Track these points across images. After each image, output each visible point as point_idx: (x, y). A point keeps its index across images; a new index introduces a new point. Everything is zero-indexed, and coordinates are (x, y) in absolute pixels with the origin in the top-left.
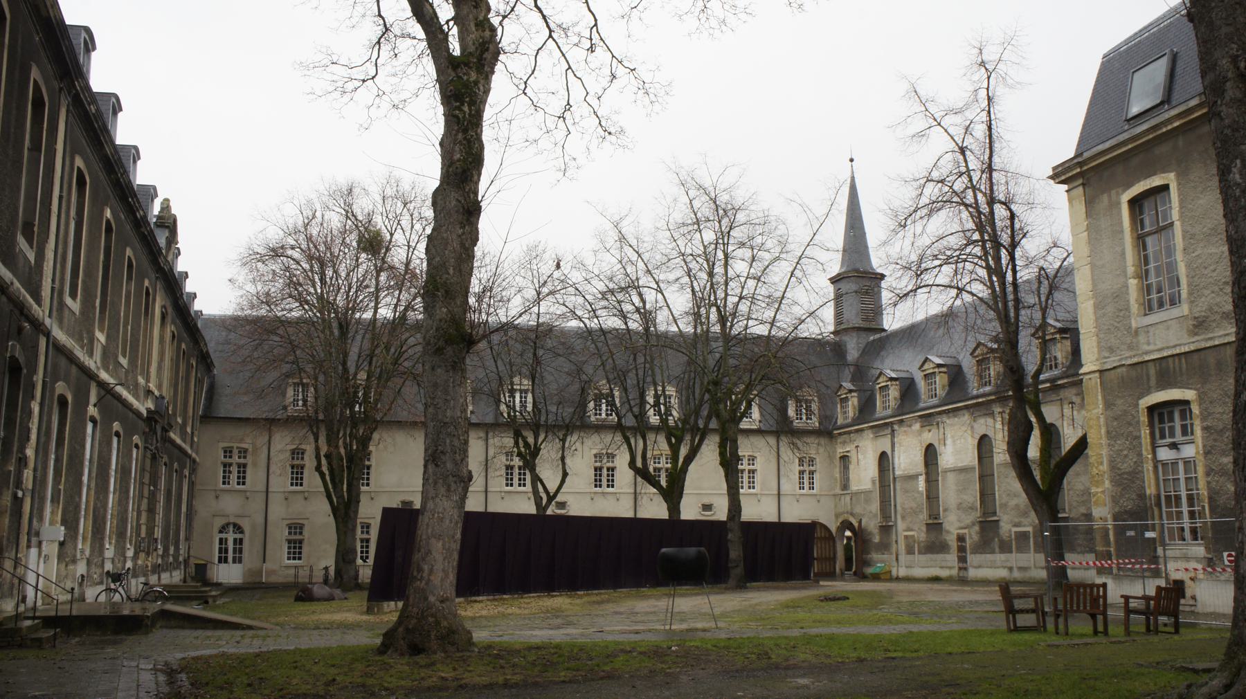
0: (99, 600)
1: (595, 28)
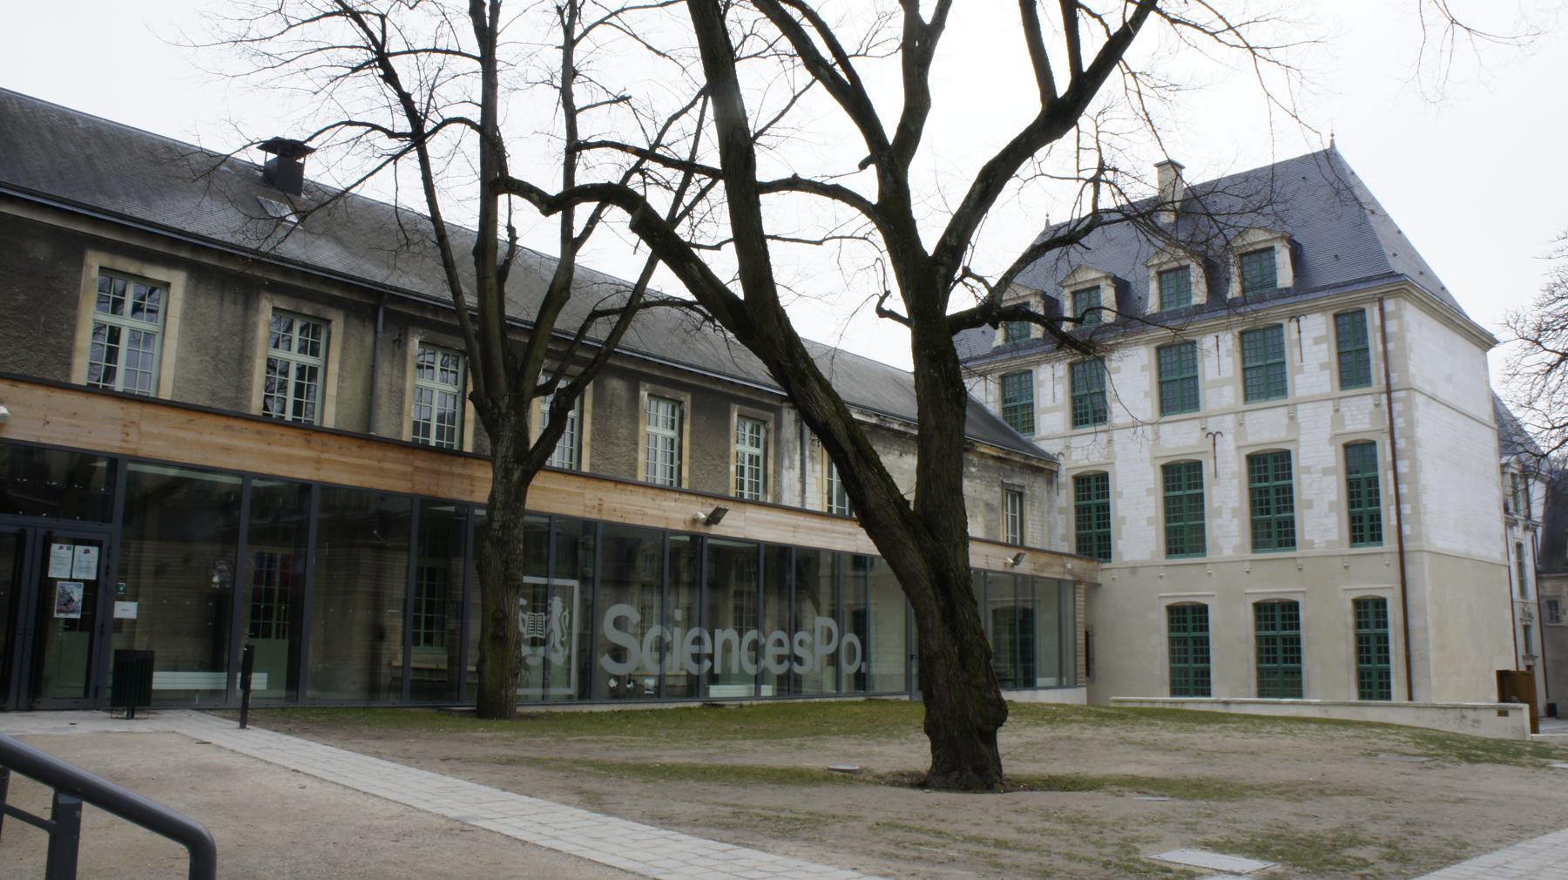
0: (590, 333)
1: (890, 122)
